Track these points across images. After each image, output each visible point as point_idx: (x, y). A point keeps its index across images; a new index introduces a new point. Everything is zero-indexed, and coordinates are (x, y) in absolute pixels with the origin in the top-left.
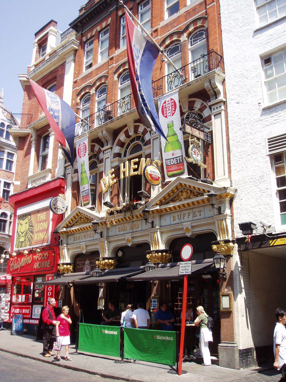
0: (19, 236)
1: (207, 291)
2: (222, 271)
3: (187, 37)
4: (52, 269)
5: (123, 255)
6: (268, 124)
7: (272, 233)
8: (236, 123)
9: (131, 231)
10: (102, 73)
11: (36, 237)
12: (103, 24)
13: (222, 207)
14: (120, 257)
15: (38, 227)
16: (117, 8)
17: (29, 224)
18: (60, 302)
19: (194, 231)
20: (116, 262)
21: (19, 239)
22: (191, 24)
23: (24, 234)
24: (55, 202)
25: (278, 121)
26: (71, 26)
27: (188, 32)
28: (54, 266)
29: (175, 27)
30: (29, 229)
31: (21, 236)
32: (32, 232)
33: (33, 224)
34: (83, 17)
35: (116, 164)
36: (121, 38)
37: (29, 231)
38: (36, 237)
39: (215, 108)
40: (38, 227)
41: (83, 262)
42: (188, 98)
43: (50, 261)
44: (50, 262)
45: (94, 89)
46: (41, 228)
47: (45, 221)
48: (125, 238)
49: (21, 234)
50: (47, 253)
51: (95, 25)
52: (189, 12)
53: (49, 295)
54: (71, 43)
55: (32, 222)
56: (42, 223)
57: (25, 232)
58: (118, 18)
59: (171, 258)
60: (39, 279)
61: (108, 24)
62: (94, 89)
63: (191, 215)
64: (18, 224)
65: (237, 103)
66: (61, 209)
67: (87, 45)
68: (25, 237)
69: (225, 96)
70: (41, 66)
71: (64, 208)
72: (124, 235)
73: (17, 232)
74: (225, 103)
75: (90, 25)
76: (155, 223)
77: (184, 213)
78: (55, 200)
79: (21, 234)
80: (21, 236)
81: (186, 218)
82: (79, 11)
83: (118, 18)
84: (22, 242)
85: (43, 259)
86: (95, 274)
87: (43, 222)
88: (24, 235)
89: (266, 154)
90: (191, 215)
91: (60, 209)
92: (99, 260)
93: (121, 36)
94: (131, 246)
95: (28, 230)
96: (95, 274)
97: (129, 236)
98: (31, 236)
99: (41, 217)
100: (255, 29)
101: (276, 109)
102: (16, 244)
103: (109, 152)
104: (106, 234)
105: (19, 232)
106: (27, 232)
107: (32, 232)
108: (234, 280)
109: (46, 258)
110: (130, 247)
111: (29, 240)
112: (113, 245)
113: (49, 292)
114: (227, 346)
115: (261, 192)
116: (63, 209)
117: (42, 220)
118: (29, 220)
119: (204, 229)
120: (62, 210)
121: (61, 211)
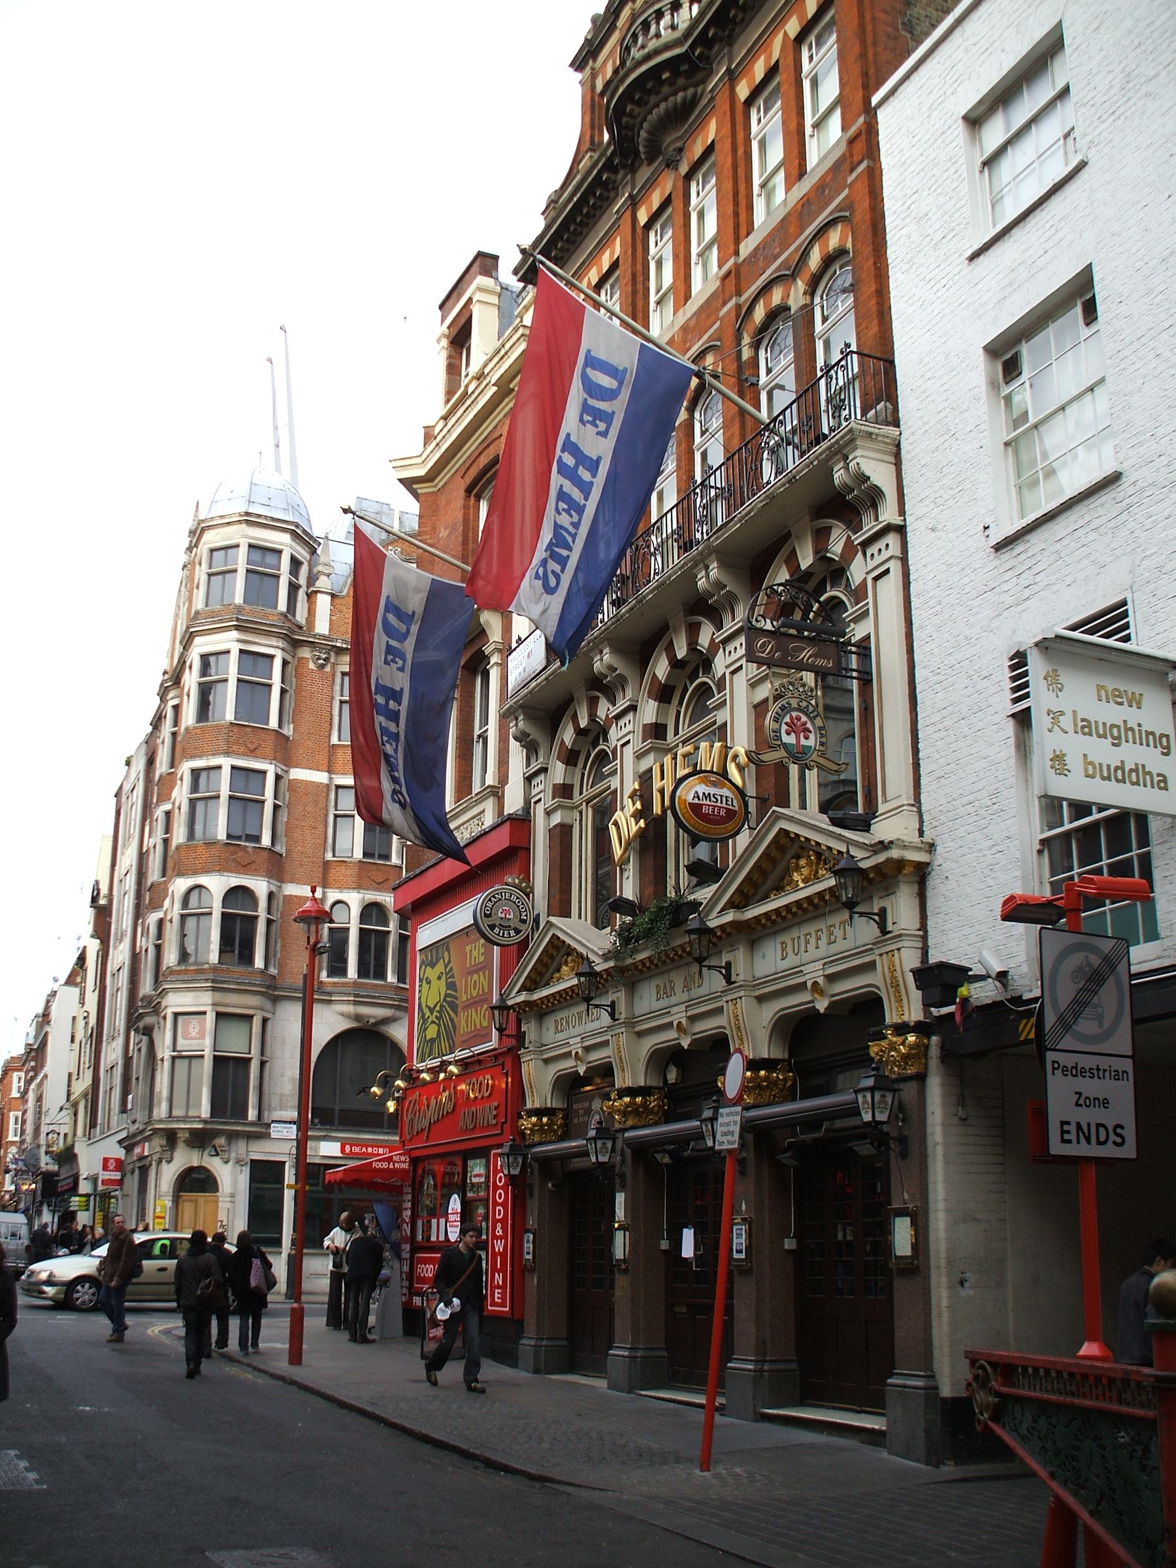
0: (424, 1019)
1: (226, 1246)
2: (617, 1170)
3: (805, 293)
4: (502, 1130)
5: (682, 1075)
6: (1009, 601)
7: (1021, 997)
8: (931, 603)
9: (685, 997)
10: (768, 272)
11: (463, 1023)
12: (604, 257)
13: (889, 911)
14: (672, 1084)
15: (466, 992)
16: (729, 71)
17: (447, 979)
18: (739, 1235)
19: (696, 1031)
20: (663, 1101)
21: (426, 1029)
22: (705, 355)
23: (435, 1013)
24: (490, 904)
25: (1036, 588)
26: (519, 275)
27: (806, 276)
28: (506, 1122)
29: (776, 257)
30: (447, 995)
31: (430, 1020)
32: (454, 1007)
33: (456, 979)
34: (545, 240)
35: (645, 764)
36: (652, 305)
37: (448, 1003)
38: (463, 1023)
39: (876, 554)
40: (466, 992)
41: (586, 1104)
42: (811, 521)
43: (496, 1104)
44: (496, 1108)
45: (801, 285)
46: (474, 994)
47: (483, 969)
48: (571, 1052)
49: (428, 1013)
50: (488, 1077)
51: (583, 263)
52: (808, 200)
53: (497, 1217)
54: (518, 339)
55: (454, 971)
56: (475, 977)
57: (438, 1008)
58: (739, 108)
59: (794, 1086)
60: (475, 1165)
61: (773, 62)
62: (801, 285)
63: (824, 937)
64: (421, 980)
65: (933, 530)
66: (513, 926)
67: (759, 111)
68: (439, 1026)
69: (902, 512)
70: (453, 426)
71: (524, 922)
72: (669, 1012)
73: (420, 1005)
74: (901, 530)
75: (758, 28)
76: (736, 970)
77: (807, 932)
78: (490, 900)
79: (428, 1013)
80: (430, 1020)
81: (813, 953)
82: (543, 214)
83: (739, 108)
84: (432, 1040)
85: (480, 1097)
86: (864, 1097)
87: (477, 971)
88: (436, 1017)
89: (1004, 715)
90: (824, 937)
91: (510, 926)
92: (610, 1100)
93: (653, 298)
94: (691, 1048)
95: (444, 1000)
96: (864, 1097)
97: (679, 1016)
98: (451, 1020)
99: (475, 953)
100: (969, 253)
101: (1028, 545)
102: (418, 1049)
103: (741, 644)
104: (626, 1011)
105: (424, 1006)
106: (442, 1006)
107: (454, 1007)
108: (930, 1159)
109: (486, 1094)
110: (824, 1014)
111: (449, 1037)
112: (649, 1044)
113: (498, 1208)
114: (905, 1386)
115: (994, 850)
116: (523, 927)
117: (476, 965)
118: (446, 967)
119: (567, 1066)
120: (517, 931)
121: (512, 933)
